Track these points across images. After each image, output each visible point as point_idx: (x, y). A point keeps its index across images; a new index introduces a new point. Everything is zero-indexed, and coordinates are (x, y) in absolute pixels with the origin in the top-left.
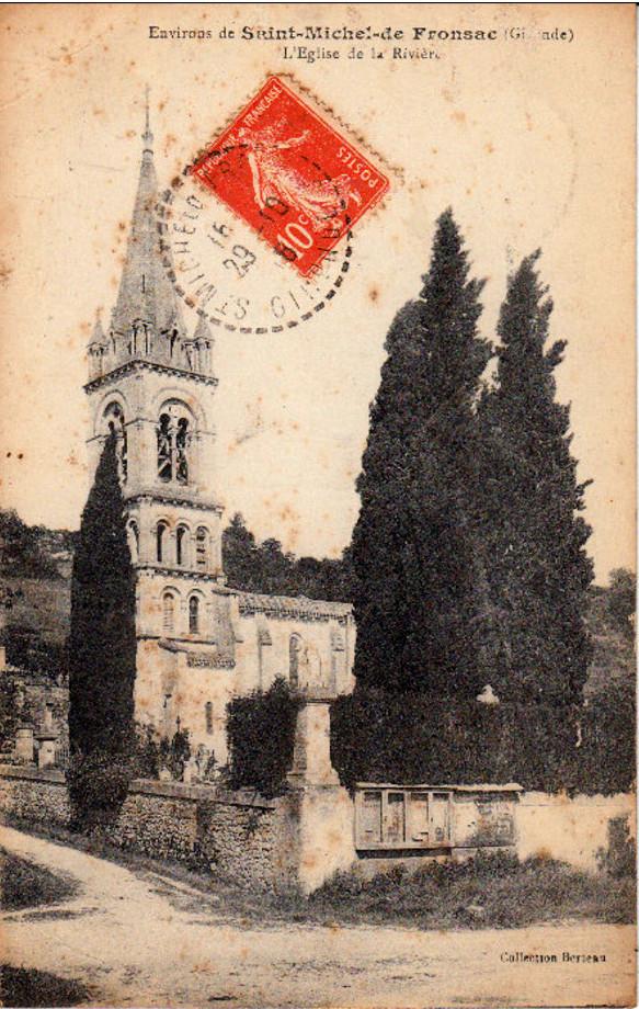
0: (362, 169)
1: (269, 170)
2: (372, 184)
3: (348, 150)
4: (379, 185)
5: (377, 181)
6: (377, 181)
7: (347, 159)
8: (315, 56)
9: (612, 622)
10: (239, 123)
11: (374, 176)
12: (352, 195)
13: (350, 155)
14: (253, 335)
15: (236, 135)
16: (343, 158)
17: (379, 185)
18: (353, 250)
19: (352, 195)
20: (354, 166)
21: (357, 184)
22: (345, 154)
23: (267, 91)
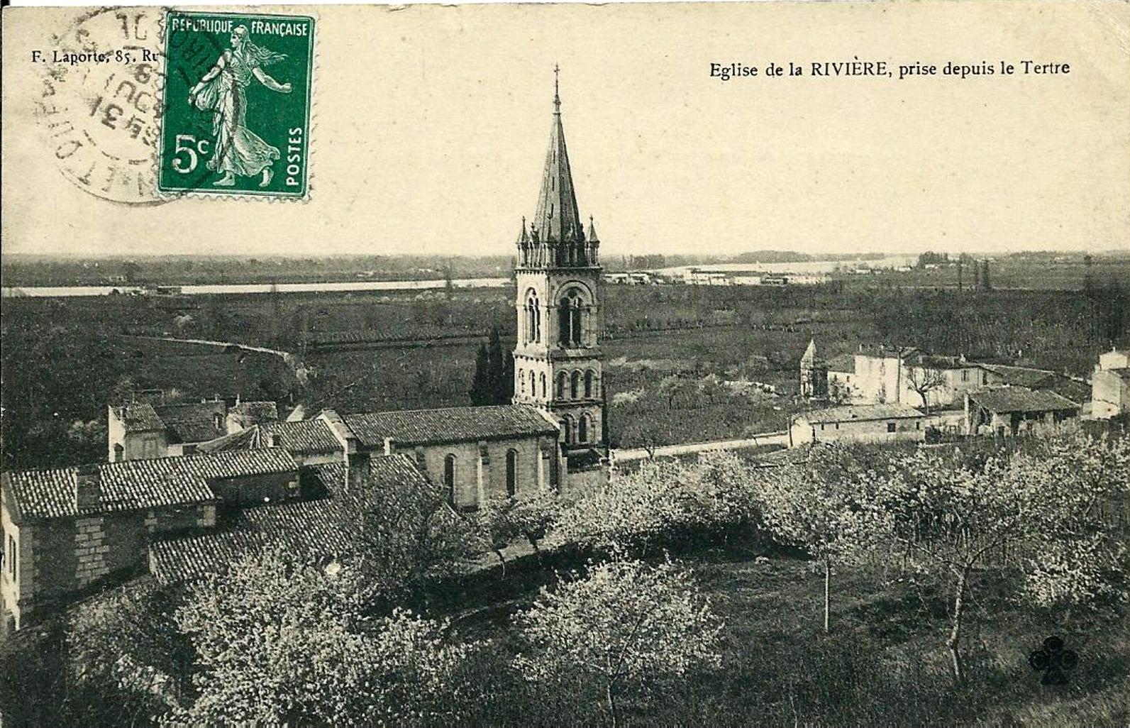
0: (295, 162)
1: (227, 80)
2: (291, 182)
3: (302, 136)
4: (292, 189)
5: (297, 184)
6: (297, 184)
7: (295, 141)
8: (730, 73)
9: (105, 596)
10: (247, 22)
11: (298, 178)
12: (265, 172)
13: (299, 142)
14: (90, 136)
15: (235, 25)
16: (293, 137)
17: (292, 189)
18: (145, 145)
19: (265, 172)
20: (293, 153)
21: (279, 168)
22: (296, 137)
23: (297, 22)
